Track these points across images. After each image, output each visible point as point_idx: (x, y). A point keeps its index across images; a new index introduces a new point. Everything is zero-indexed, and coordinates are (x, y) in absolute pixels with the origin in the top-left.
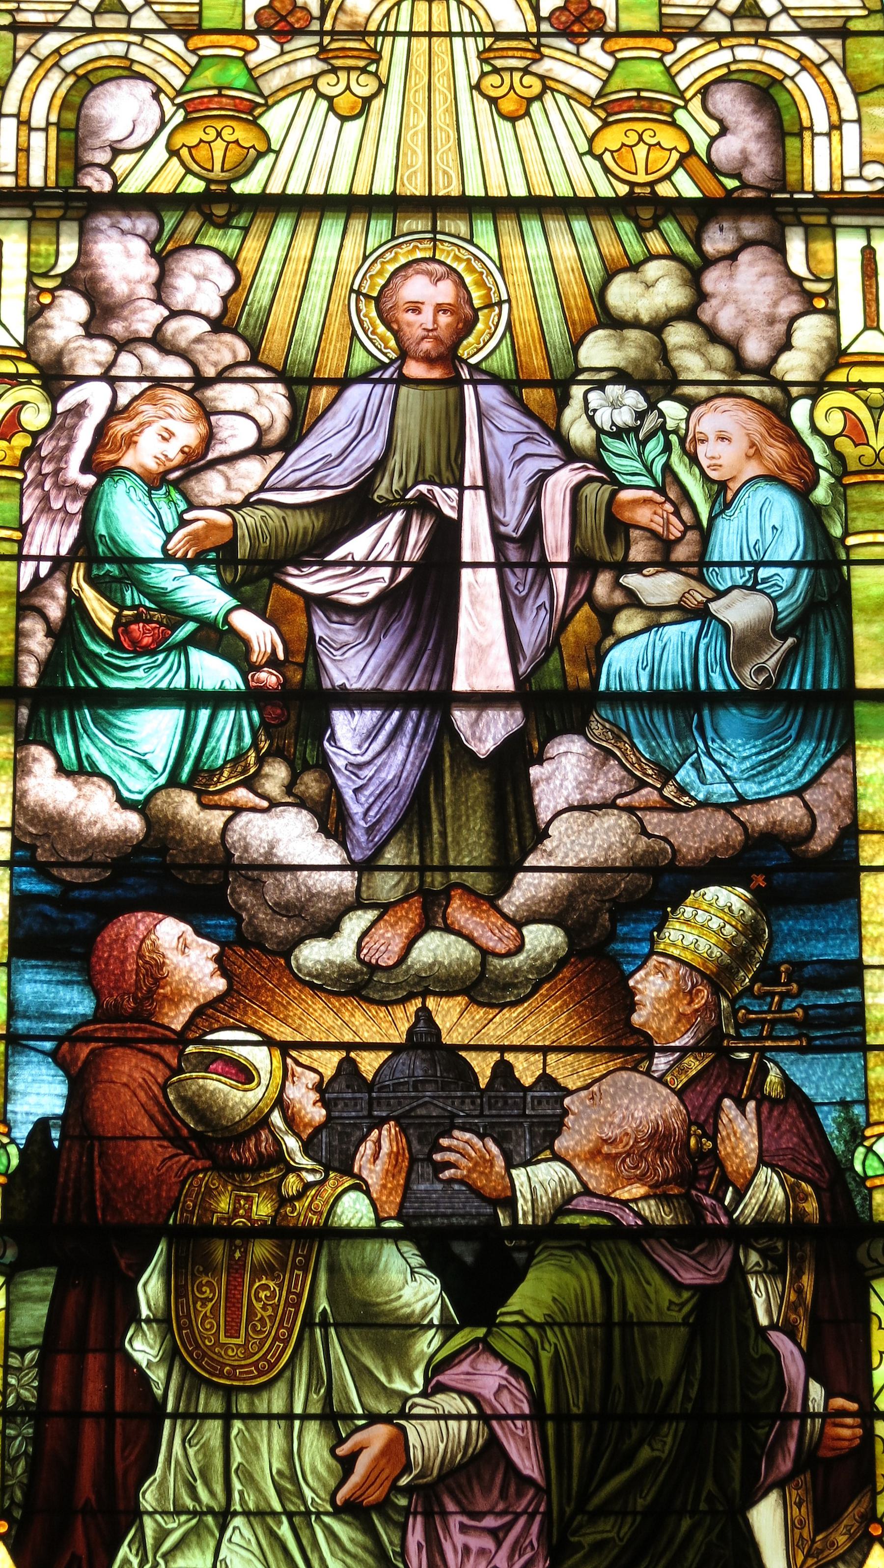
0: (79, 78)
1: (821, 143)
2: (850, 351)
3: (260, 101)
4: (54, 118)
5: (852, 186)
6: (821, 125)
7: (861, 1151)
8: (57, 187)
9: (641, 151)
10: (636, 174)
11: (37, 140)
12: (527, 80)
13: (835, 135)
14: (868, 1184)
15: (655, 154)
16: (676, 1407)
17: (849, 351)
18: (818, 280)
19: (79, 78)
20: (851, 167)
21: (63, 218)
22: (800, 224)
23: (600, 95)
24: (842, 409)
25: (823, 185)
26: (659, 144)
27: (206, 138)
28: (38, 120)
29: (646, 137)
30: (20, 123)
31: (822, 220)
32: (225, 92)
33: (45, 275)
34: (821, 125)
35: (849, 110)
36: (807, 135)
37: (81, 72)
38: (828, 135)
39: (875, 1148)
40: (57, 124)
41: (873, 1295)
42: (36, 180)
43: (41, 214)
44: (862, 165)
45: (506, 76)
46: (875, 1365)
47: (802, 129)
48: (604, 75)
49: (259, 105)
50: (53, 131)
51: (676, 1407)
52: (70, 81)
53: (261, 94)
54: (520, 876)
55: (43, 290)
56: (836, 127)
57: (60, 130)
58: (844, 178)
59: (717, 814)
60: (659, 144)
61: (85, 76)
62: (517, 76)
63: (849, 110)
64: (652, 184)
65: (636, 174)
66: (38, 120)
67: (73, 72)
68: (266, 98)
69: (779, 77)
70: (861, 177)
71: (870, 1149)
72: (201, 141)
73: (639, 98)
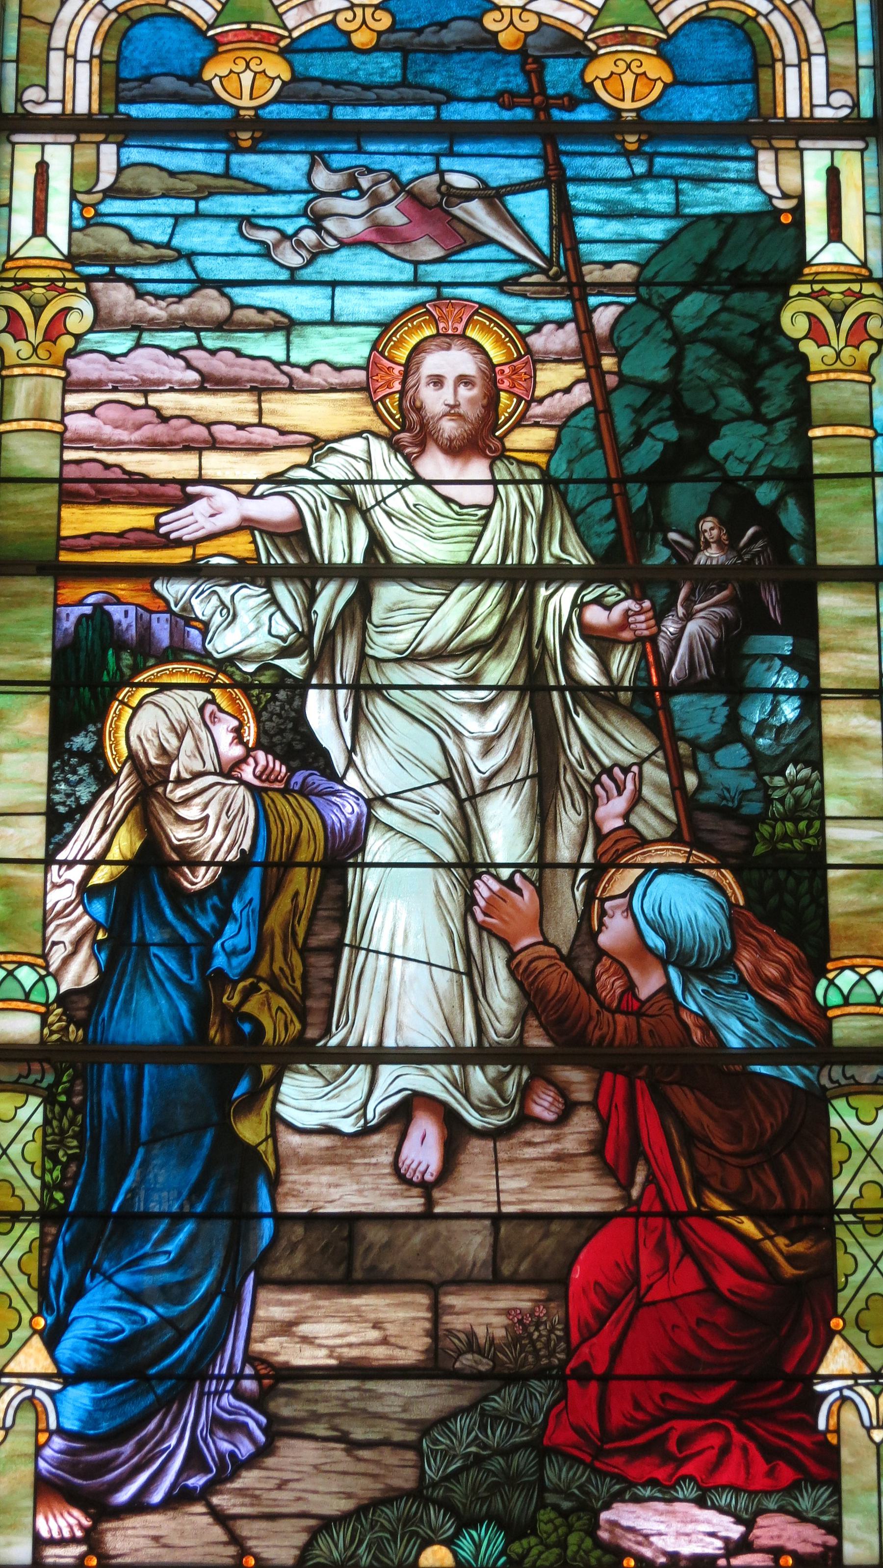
0: (120, 15)
1: (792, 74)
2: (816, 261)
3: (286, 34)
4: (97, 52)
5: (820, 113)
6: (791, 56)
7: (823, 983)
8: (100, 112)
9: (628, 79)
10: (623, 100)
11: (83, 70)
12: (526, 15)
13: (805, 66)
14: (830, 1014)
15: (261, 81)
16: (303, 856)
17: (815, 261)
18: (785, 196)
19: (120, 15)
20: (820, 96)
21: (105, 141)
22: (772, 148)
23: (591, 30)
24: (809, 315)
25: (793, 111)
26: (644, 73)
27: (618, 70)
28: (83, 54)
29: (633, 66)
30: (66, 56)
31: (791, 144)
32: (254, 26)
33: (89, 192)
34: (791, 56)
35: (817, 47)
36: (779, 66)
37: (121, 9)
38: (799, 66)
39: (837, 981)
40: (100, 56)
41: (831, 1110)
42: (82, 108)
43: (85, 137)
44: (829, 93)
45: (359, 11)
46: (835, 1173)
47: (774, 60)
48: (281, 10)
49: (283, 37)
50: (96, 61)
51: (303, 856)
52: (113, 16)
53: (285, 27)
54: (552, 473)
55: (84, 206)
56: (805, 57)
57: (102, 62)
58: (812, 106)
59: (677, 708)
60: (644, 73)
61: (126, 13)
62: (369, 11)
63: (817, 47)
64: (256, 109)
65: (623, 100)
66: (83, 54)
67: (115, 9)
68: (290, 31)
69: (751, 13)
70: (828, 105)
71: (831, 982)
72: (231, 71)
73: (627, 31)
